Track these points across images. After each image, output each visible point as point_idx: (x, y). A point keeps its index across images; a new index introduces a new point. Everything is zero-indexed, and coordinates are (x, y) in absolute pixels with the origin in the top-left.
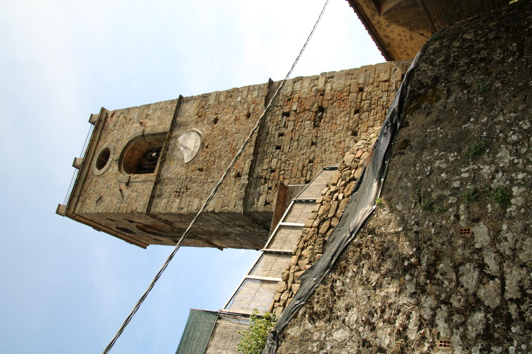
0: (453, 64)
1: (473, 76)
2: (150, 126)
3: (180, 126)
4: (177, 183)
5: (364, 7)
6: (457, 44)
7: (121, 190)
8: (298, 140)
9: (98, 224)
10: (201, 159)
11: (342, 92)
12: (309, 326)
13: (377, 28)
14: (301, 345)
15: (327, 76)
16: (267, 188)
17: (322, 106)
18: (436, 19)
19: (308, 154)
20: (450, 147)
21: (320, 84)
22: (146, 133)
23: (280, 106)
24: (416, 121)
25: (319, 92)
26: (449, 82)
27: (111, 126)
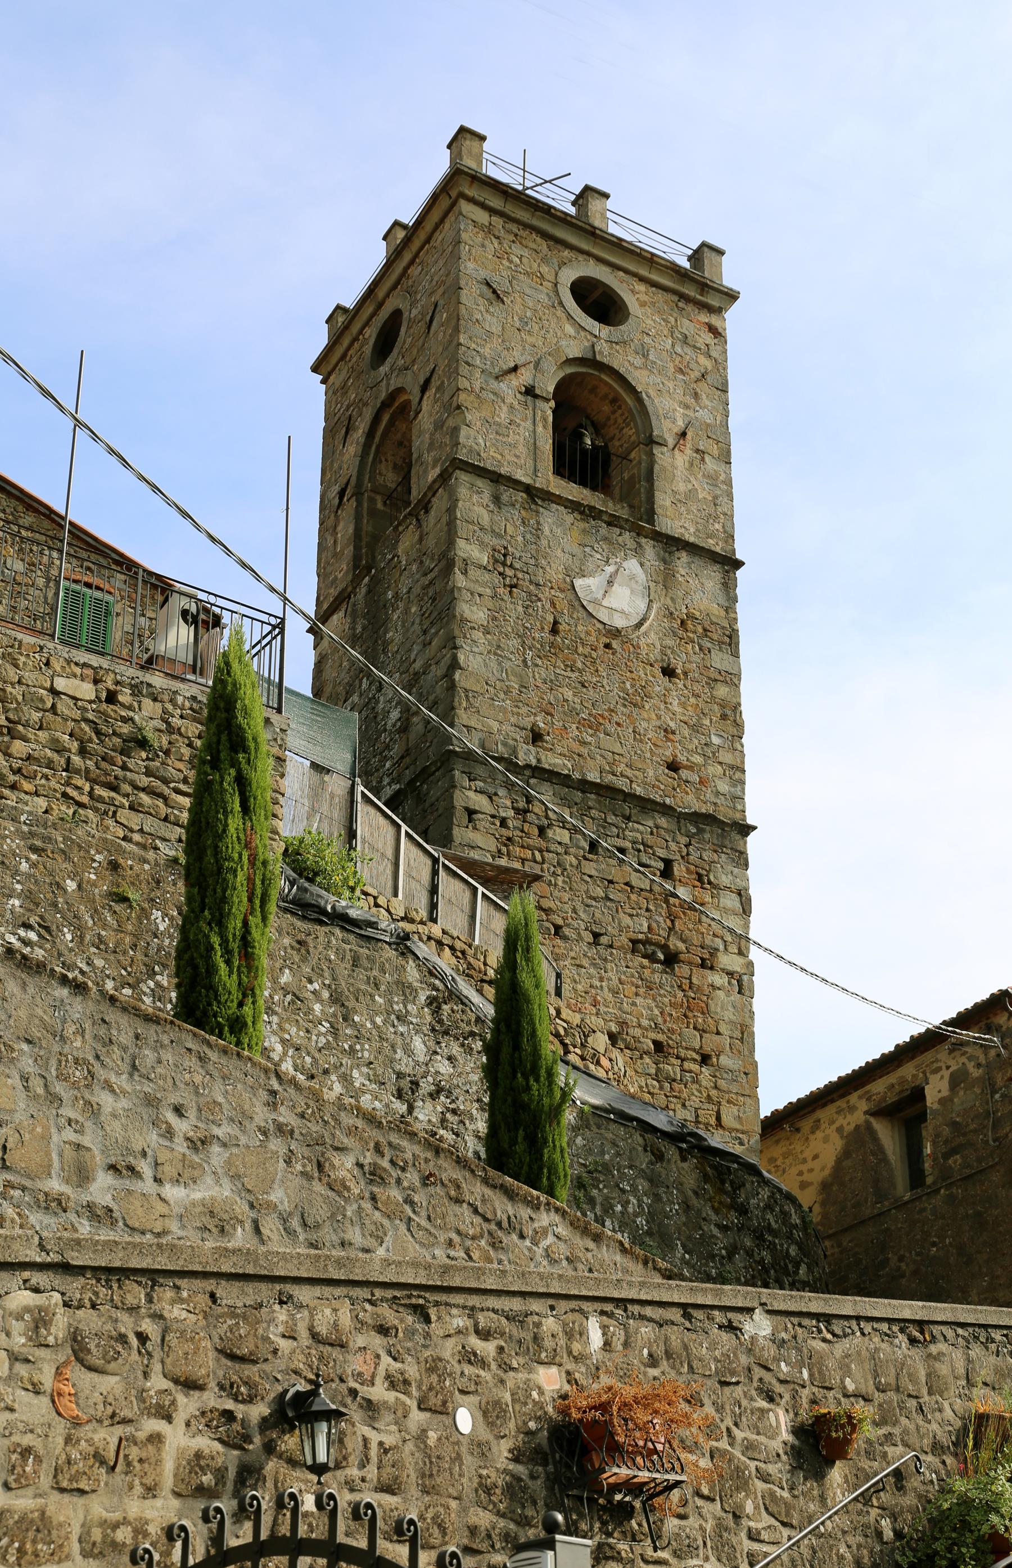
0: (764, 1241)
1: (745, 1268)
2: (673, 466)
3: (665, 561)
4: (526, 557)
5: (892, 1078)
6: (793, 1251)
7: (515, 369)
8: (607, 898)
9: (417, 255)
10: (580, 628)
11: (705, 1012)
12: (422, 998)
13: (838, 1103)
14: (398, 983)
15: (745, 978)
16: (504, 815)
17: (679, 961)
18: (839, 1245)
19: (575, 923)
20: (653, 1220)
21: (728, 960)
22: (656, 450)
23: (688, 854)
24: (684, 1172)
25: (711, 954)
26: (739, 1230)
27: (687, 326)
